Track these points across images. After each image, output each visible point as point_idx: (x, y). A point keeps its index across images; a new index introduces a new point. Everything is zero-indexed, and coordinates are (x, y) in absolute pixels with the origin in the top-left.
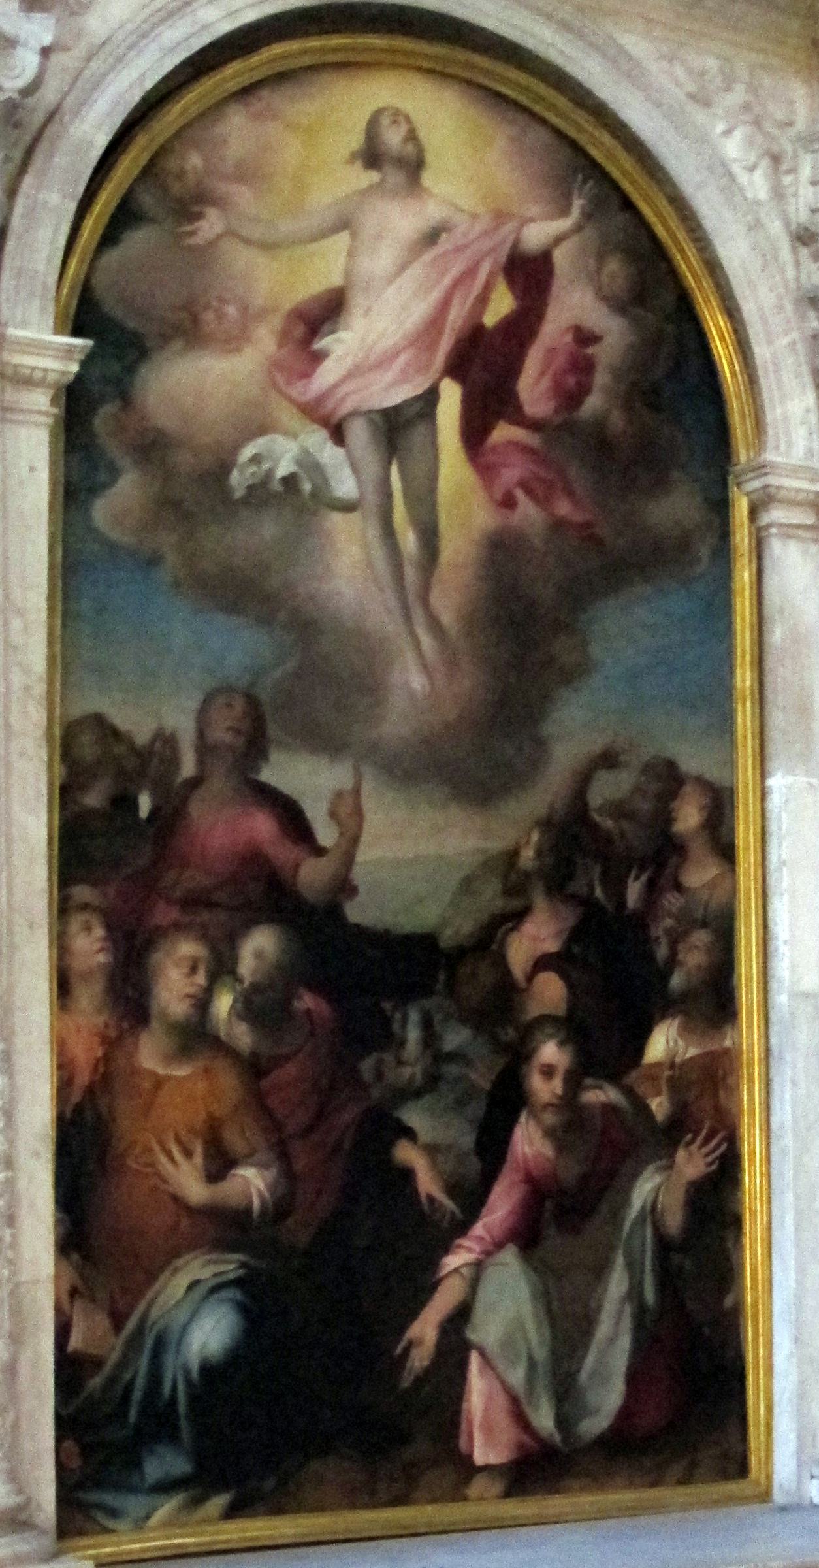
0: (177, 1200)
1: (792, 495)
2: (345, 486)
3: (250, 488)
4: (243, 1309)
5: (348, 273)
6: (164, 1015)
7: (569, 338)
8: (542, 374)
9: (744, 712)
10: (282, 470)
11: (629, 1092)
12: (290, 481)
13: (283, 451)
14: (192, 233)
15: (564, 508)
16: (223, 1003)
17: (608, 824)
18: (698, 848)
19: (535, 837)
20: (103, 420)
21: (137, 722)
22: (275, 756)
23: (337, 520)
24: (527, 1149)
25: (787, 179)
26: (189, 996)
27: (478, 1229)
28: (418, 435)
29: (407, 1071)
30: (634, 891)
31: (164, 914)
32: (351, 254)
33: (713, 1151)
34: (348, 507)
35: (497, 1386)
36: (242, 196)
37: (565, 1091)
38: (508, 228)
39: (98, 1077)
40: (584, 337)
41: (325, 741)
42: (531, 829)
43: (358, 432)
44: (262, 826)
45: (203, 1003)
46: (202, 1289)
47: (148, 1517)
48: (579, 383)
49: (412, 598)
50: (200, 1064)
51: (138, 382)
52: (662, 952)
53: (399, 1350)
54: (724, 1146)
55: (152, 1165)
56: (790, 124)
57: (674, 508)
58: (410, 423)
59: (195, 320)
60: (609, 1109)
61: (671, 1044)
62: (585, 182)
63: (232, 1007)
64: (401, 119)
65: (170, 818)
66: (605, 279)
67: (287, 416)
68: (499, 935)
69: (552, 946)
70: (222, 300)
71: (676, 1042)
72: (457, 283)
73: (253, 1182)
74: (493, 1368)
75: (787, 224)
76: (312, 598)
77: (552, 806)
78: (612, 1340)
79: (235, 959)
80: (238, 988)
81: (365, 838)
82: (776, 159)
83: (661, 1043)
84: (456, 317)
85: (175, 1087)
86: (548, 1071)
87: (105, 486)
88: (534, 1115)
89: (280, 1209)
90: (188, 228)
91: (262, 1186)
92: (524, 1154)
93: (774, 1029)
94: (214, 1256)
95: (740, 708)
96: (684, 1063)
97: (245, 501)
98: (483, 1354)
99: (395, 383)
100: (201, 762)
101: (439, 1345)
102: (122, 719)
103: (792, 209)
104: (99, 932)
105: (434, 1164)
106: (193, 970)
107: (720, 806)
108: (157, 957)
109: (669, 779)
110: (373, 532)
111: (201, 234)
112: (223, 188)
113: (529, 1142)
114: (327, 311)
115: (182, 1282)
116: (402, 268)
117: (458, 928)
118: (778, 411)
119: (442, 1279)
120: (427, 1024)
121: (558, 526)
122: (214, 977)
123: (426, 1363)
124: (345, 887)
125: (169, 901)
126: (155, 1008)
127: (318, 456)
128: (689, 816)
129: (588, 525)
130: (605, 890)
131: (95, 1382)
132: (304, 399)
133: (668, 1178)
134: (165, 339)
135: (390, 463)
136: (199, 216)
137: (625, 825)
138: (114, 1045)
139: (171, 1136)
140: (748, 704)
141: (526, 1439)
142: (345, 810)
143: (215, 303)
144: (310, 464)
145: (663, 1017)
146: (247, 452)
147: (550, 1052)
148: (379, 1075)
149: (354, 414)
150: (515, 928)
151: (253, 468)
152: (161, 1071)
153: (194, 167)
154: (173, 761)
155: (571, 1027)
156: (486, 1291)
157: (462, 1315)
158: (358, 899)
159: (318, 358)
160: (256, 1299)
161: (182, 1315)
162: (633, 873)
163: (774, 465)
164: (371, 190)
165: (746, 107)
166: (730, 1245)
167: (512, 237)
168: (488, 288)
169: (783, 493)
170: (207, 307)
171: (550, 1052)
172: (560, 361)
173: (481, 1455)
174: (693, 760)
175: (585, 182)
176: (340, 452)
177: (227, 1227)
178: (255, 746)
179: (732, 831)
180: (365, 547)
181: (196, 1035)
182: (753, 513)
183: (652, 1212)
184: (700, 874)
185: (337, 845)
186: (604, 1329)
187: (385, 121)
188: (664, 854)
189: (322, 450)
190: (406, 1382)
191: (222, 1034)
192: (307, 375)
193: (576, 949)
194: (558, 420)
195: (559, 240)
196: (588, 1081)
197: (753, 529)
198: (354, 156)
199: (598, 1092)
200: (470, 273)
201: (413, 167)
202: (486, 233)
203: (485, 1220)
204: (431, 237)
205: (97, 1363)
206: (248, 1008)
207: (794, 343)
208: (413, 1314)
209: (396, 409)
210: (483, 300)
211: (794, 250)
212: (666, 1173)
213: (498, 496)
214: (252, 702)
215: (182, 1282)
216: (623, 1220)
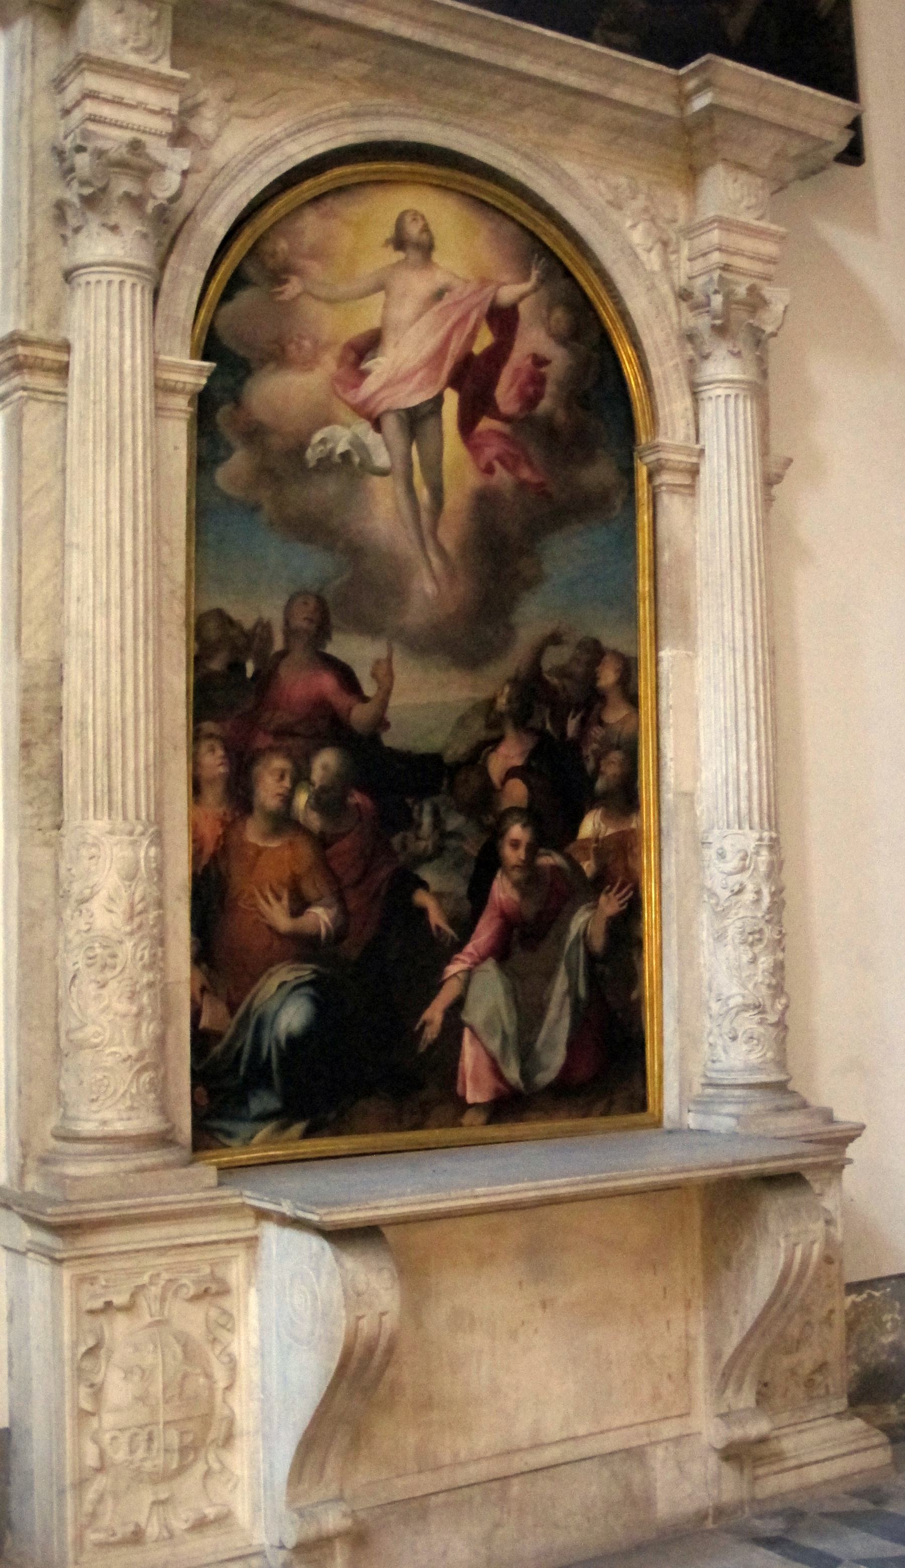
0: (280, 936)
2: (382, 459)
4: (315, 1000)
5: (384, 319)
6: (262, 807)
7: (529, 362)
8: (512, 385)
10: (340, 449)
11: (569, 858)
12: (346, 456)
13: (341, 437)
14: (281, 293)
15: (526, 473)
16: (302, 799)
17: (555, 681)
18: (614, 697)
19: (507, 690)
21: (245, 615)
22: (336, 637)
23: (376, 482)
25: (673, 257)
26: (279, 795)
27: (469, 948)
29: (422, 844)
30: (572, 725)
31: (262, 741)
32: (385, 307)
34: (384, 473)
35: (482, 1051)
36: (314, 268)
37: (527, 857)
38: (489, 290)
41: (368, 627)
44: (327, 683)
45: (288, 799)
46: (288, 987)
47: (252, 1137)
48: (535, 391)
49: (426, 532)
52: (590, 765)
53: (417, 1028)
54: (631, 893)
55: (255, 906)
57: (598, 473)
58: (424, 418)
59: (283, 350)
60: (555, 869)
62: (539, 259)
63: (307, 802)
65: (266, 678)
66: (553, 323)
67: (344, 413)
69: (518, 762)
70: (300, 336)
73: (321, 917)
74: (479, 1040)
75: (673, 287)
76: (360, 532)
77: (518, 670)
78: (557, 1021)
79: (309, 770)
81: (395, 690)
82: (665, 244)
83: (591, 825)
84: (455, 348)
86: (515, 844)
88: (506, 873)
89: (339, 935)
90: (279, 289)
94: (296, 966)
96: (605, 839)
97: (316, 469)
98: (472, 1030)
99: (410, 395)
100: (287, 641)
102: (236, 612)
103: (675, 277)
104: (220, 752)
106: (282, 777)
107: (628, 670)
108: (258, 769)
109: (595, 652)
110: (400, 489)
111: (287, 293)
112: (301, 263)
113: (503, 890)
114: (368, 345)
115: (274, 982)
116: (419, 316)
117: (456, 750)
118: (667, 410)
120: (436, 813)
121: (522, 485)
122: (295, 783)
123: (435, 1036)
124: (382, 723)
126: (257, 802)
127: (364, 439)
128: (608, 677)
129: (542, 484)
131: (218, 1049)
134: (263, 362)
135: (411, 444)
136: (286, 281)
137: (566, 682)
138: (230, 827)
141: (501, 1086)
142: (381, 672)
143: (296, 339)
144: (358, 445)
146: (317, 437)
147: (517, 831)
148: (404, 847)
149: (388, 411)
151: (321, 448)
154: (268, 640)
155: (531, 815)
156: (476, 991)
157: (458, 1004)
159: (364, 374)
160: (323, 993)
161: (274, 1005)
162: (571, 714)
163: (664, 445)
164: (399, 264)
165: (646, 210)
166: (635, 958)
167: (492, 295)
168: (476, 329)
169: (670, 464)
171: (517, 831)
172: (523, 377)
173: (471, 1097)
174: (610, 639)
175: (539, 259)
176: (378, 437)
177: (304, 946)
178: (322, 630)
179: (636, 686)
181: (283, 821)
182: (650, 476)
183: (584, 936)
184: (615, 714)
186: (552, 1013)
187: (408, 219)
188: (592, 701)
189: (366, 435)
190: (422, 1049)
191: (301, 820)
192: (356, 386)
193: (534, 764)
194: (522, 416)
195: (522, 297)
196: (542, 850)
198: (387, 242)
199: (548, 858)
200: (464, 319)
201: (426, 249)
202: (475, 292)
204: (439, 295)
205: (219, 1036)
206: (319, 802)
207: (677, 365)
208: (427, 1004)
209: (416, 408)
210: (472, 336)
211: (677, 304)
213: (483, 466)
214: (321, 601)
215: (274, 982)
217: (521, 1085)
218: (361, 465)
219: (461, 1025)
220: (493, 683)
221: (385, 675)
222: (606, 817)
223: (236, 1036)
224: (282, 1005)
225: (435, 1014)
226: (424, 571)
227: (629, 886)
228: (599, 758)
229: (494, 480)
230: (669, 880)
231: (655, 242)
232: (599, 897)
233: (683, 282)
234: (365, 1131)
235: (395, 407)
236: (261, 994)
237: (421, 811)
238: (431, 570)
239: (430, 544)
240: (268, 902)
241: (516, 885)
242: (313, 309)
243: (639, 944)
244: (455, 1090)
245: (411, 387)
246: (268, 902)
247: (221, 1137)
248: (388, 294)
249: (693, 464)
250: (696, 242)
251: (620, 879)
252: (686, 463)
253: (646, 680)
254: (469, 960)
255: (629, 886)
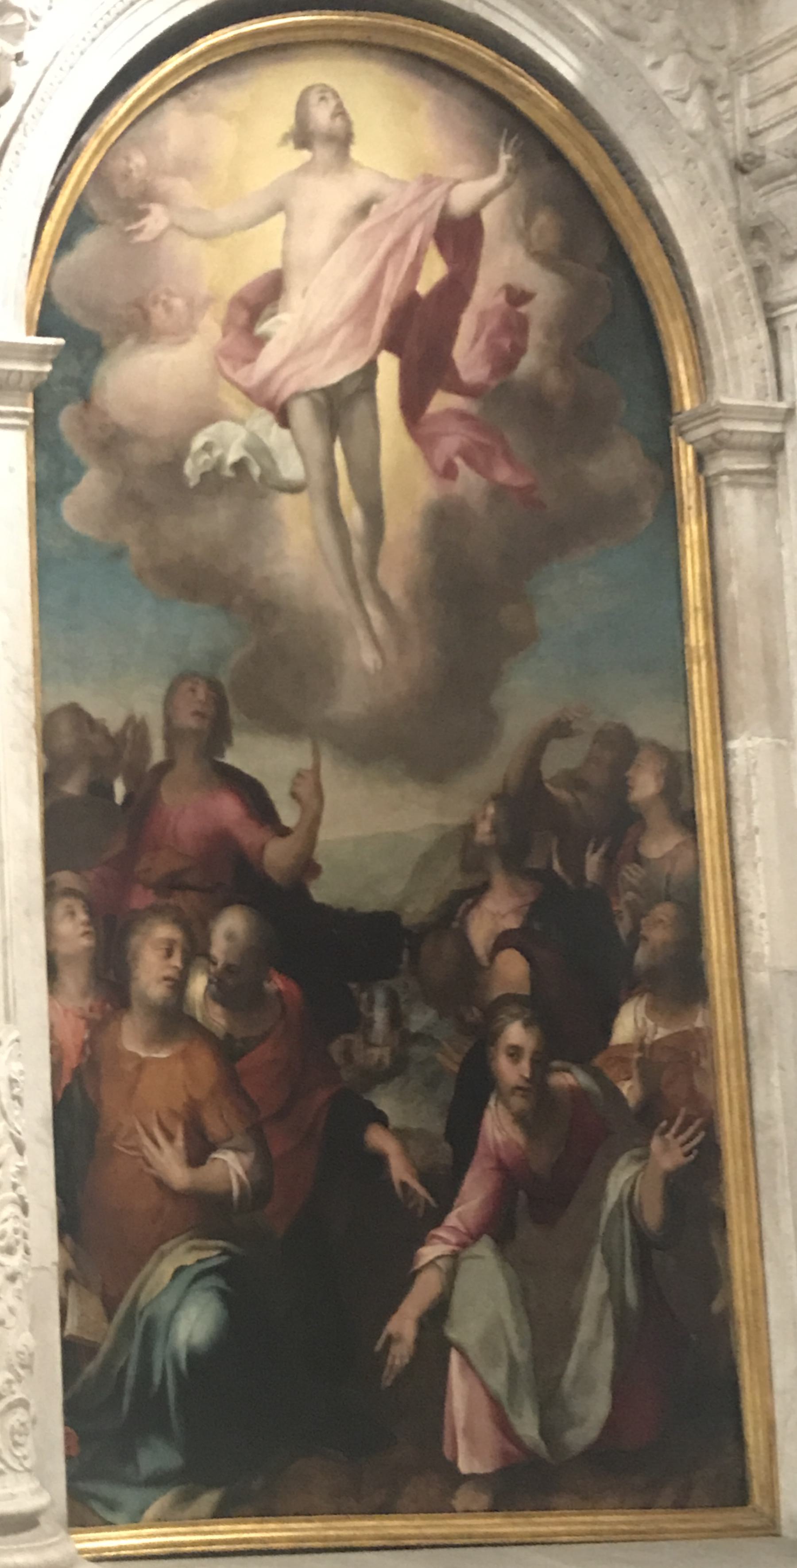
0: (161, 1184)
1: (746, 439)
2: (291, 468)
3: (204, 476)
4: (224, 1296)
5: (285, 254)
7: (501, 299)
8: (476, 339)
9: (699, 671)
10: (232, 457)
11: (596, 1074)
12: (240, 466)
13: (230, 439)
14: (139, 231)
15: (503, 474)
16: (198, 985)
17: (564, 795)
18: (657, 817)
19: (491, 810)
20: (67, 420)
21: (109, 712)
22: (240, 739)
23: (286, 503)
24: (499, 1137)
26: (166, 979)
27: (452, 1219)
28: (361, 408)
29: (376, 1052)
30: (592, 863)
31: (141, 898)
32: (287, 234)
33: (690, 1139)
34: (295, 489)
35: (480, 1393)
36: (183, 189)
37: (533, 1072)
38: (437, 192)
39: (85, 1060)
40: (517, 297)
41: (282, 723)
42: (486, 804)
43: (302, 412)
44: (228, 809)
46: (187, 1277)
47: (142, 1512)
48: (513, 346)
49: (361, 575)
50: (179, 1046)
51: (97, 380)
52: (624, 927)
53: (379, 1346)
54: (702, 1134)
55: (138, 1148)
56: (721, 48)
57: (617, 464)
58: (349, 401)
60: (577, 1093)
61: (640, 1024)
62: (509, 138)
63: (207, 989)
64: (328, 95)
66: (534, 234)
67: (233, 400)
68: (459, 915)
69: (512, 923)
70: (169, 293)
71: (645, 1024)
72: (389, 254)
73: (231, 1166)
74: (473, 1368)
75: (725, 156)
76: (267, 579)
77: (506, 780)
78: (594, 1345)
79: (208, 942)
80: (212, 969)
81: (326, 817)
82: (709, 85)
83: (629, 1024)
84: (390, 290)
85: (158, 1071)
86: (515, 1053)
87: (73, 483)
88: (503, 1099)
89: (259, 1192)
90: (134, 227)
91: (241, 1171)
92: (495, 1140)
93: (752, 1009)
94: (195, 1242)
95: (695, 668)
96: (654, 1044)
97: (198, 489)
98: (462, 1353)
99: (331, 364)
100: (169, 749)
101: (418, 1341)
102: (95, 708)
103: (728, 136)
104: (82, 917)
105: (406, 1150)
106: (169, 954)
107: (679, 773)
108: (135, 940)
109: (623, 746)
110: (321, 512)
111: (146, 230)
112: (165, 184)
113: (498, 1127)
115: (167, 1269)
116: (336, 244)
117: (418, 909)
118: (725, 352)
119: (419, 1271)
120: (393, 1002)
122: (188, 962)
123: (407, 1361)
124: (309, 867)
125: (147, 886)
127: (265, 441)
128: (645, 785)
129: (531, 488)
130: (561, 862)
131: (91, 1368)
132: (247, 384)
133: (644, 1168)
134: (120, 337)
135: (334, 441)
136: (145, 213)
137: (582, 796)
138: (99, 1027)
139: (154, 1118)
140: (704, 664)
141: (511, 1448)
142: (305, 790)
143: (163, 297)
144: (259, 449)
145: (630, 996)
146: (198, 442)
147: (515, 1033)
148: (347, 1055)
149: (297, 395)
150: (476, 903)
151: (206, 456)
152: (143, 1054)
153: (138, 166)
155: (535, 1007)
156: (465, 1288)
157: (438, 1313)
158: (323, 877)
159: (260, 342)
161: (168, 1304)
162: (591, 845)
163: (726, 408)
164: (305, 169)
165: (678, 34)
166: (715, 1244)
167: (440, 203)
168: (421, 252)
169: (735, 439)
170: (155, 302)
171: (515, 1033)
172: (493, 323)
173: (464, 1466)
174: (648, 724)
175: (509, 138)
176: (286, 433)
177: (206, 1212)
178: (218, 732)
180: (315, 528)
181: (173, 1018)
182: (700, 461)
183: (629, 1205)
184: (661, 844)
185: (299, 824)
186: (585, 1332)
187: (314, 98)
188: (622, 824)
189: (268, 433)
190: (387, 1381)
191: (199, 1016)
192: (250, 360)
193: (537, 926)
194: (494, 383)
195: (487, 199)
196: (556, 1064)
197: (702, 478)
198: (285, 138)
199: (568, 1075)
200: (401, 242)
201: (342, 141)
202: (417, 200)
203: (459, 1209)
204: (363, 210)
205: (92, 1350)
206: (220, 991)
207: (741, 277)
208: (392, 1307)
209: (338, 386)
210: (415, 269)
211: (734, 179)
212: (643, 1163)
213: (440, 464)
214: (214, 686)
215: (167, 1269)
216: (599, 1214)
217: (543, 1449)
218: (262, 477)
219: (447, 1345)
220: (467, 802)
221: (310, 792)
222: (651, 1009)
223: (115, 1350)
224: (178, 1308)
225: (404, 1324)
226: (361, 634)
227: (698, 1122)
228: (637, 916)
229: (457, 488)
230: (770, 1116)
231: (692, 87)
232: (650, 1138)
233: (739, 145)
234: (307, 1512)
235: (307, 388)
236: (151, 1283)
237: (371, 1001)
238: (369, 627)
239: (366, 588)
240: (155, 1142)
241: (519, 1119)
242: (185, 250)
243: (718, 1219)
244: (444, 1457)
245: (329, 353)
246: (155, 1142)
247: (97, 1506)
248: (289, 219)
249: (775, 435)
250: (765, 73)
251: (683, 1111)
252: (763, 433)
253: (707, 789)
254: (453, 1239)
255: (698, 1122)
